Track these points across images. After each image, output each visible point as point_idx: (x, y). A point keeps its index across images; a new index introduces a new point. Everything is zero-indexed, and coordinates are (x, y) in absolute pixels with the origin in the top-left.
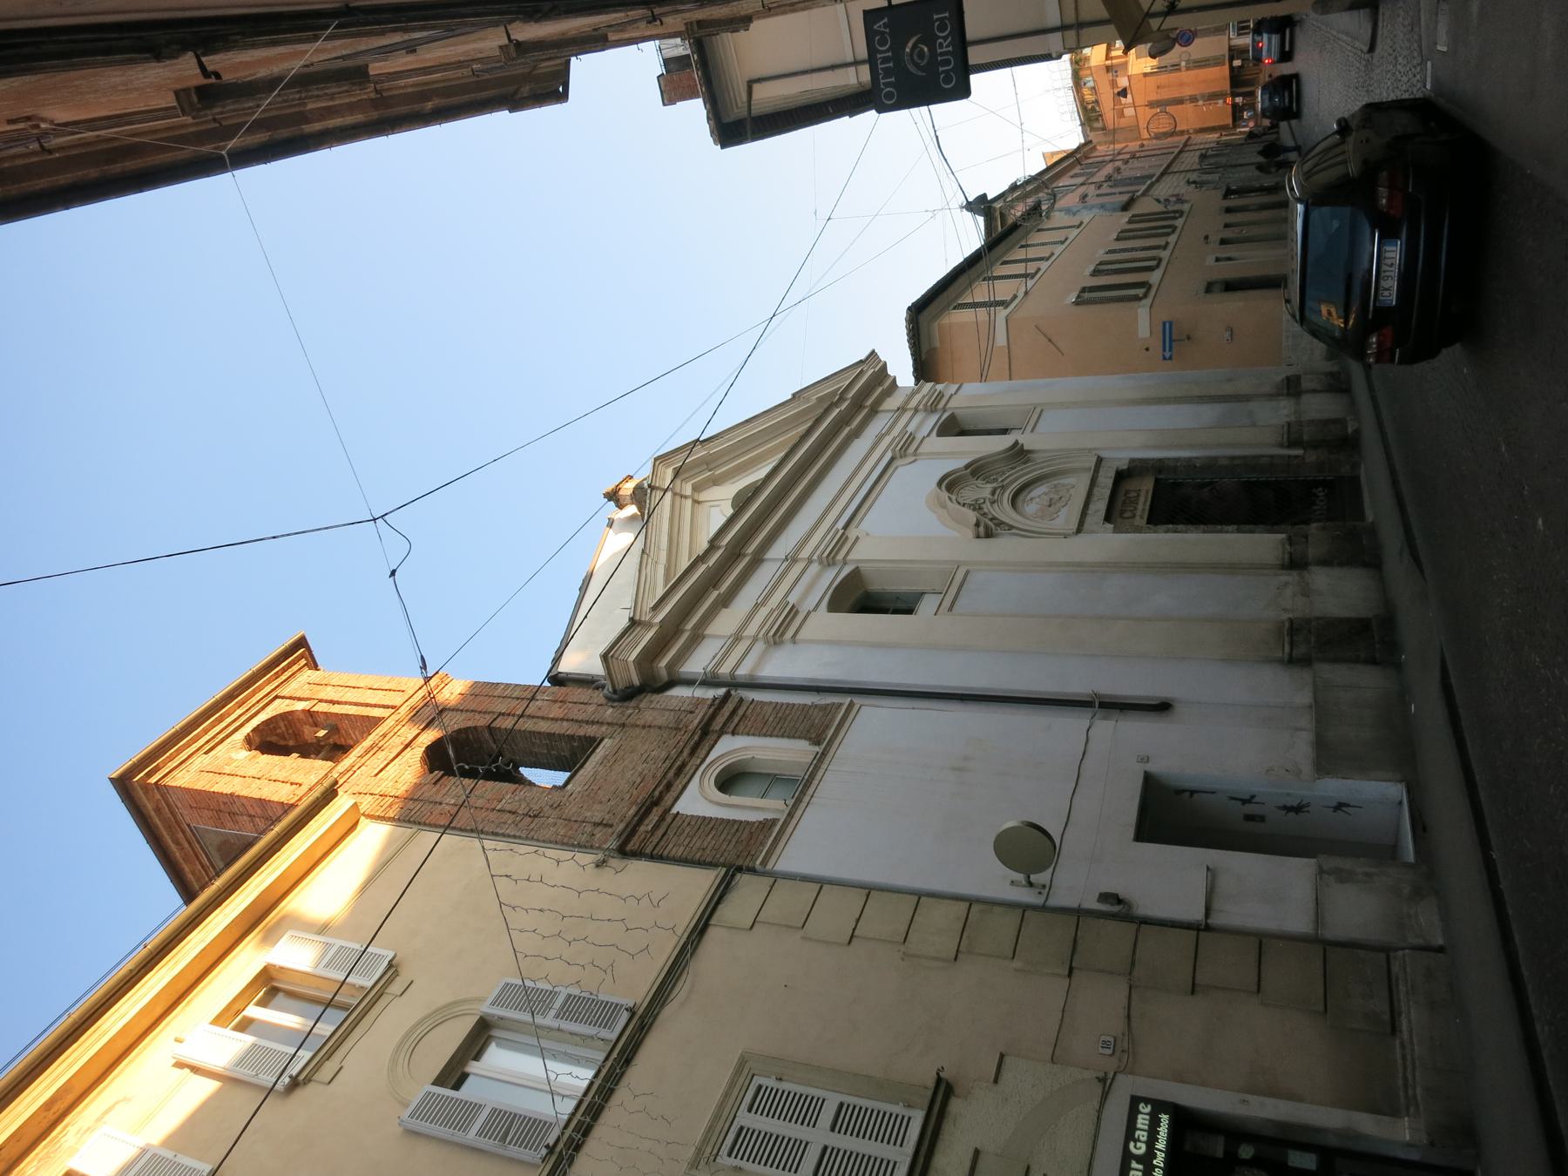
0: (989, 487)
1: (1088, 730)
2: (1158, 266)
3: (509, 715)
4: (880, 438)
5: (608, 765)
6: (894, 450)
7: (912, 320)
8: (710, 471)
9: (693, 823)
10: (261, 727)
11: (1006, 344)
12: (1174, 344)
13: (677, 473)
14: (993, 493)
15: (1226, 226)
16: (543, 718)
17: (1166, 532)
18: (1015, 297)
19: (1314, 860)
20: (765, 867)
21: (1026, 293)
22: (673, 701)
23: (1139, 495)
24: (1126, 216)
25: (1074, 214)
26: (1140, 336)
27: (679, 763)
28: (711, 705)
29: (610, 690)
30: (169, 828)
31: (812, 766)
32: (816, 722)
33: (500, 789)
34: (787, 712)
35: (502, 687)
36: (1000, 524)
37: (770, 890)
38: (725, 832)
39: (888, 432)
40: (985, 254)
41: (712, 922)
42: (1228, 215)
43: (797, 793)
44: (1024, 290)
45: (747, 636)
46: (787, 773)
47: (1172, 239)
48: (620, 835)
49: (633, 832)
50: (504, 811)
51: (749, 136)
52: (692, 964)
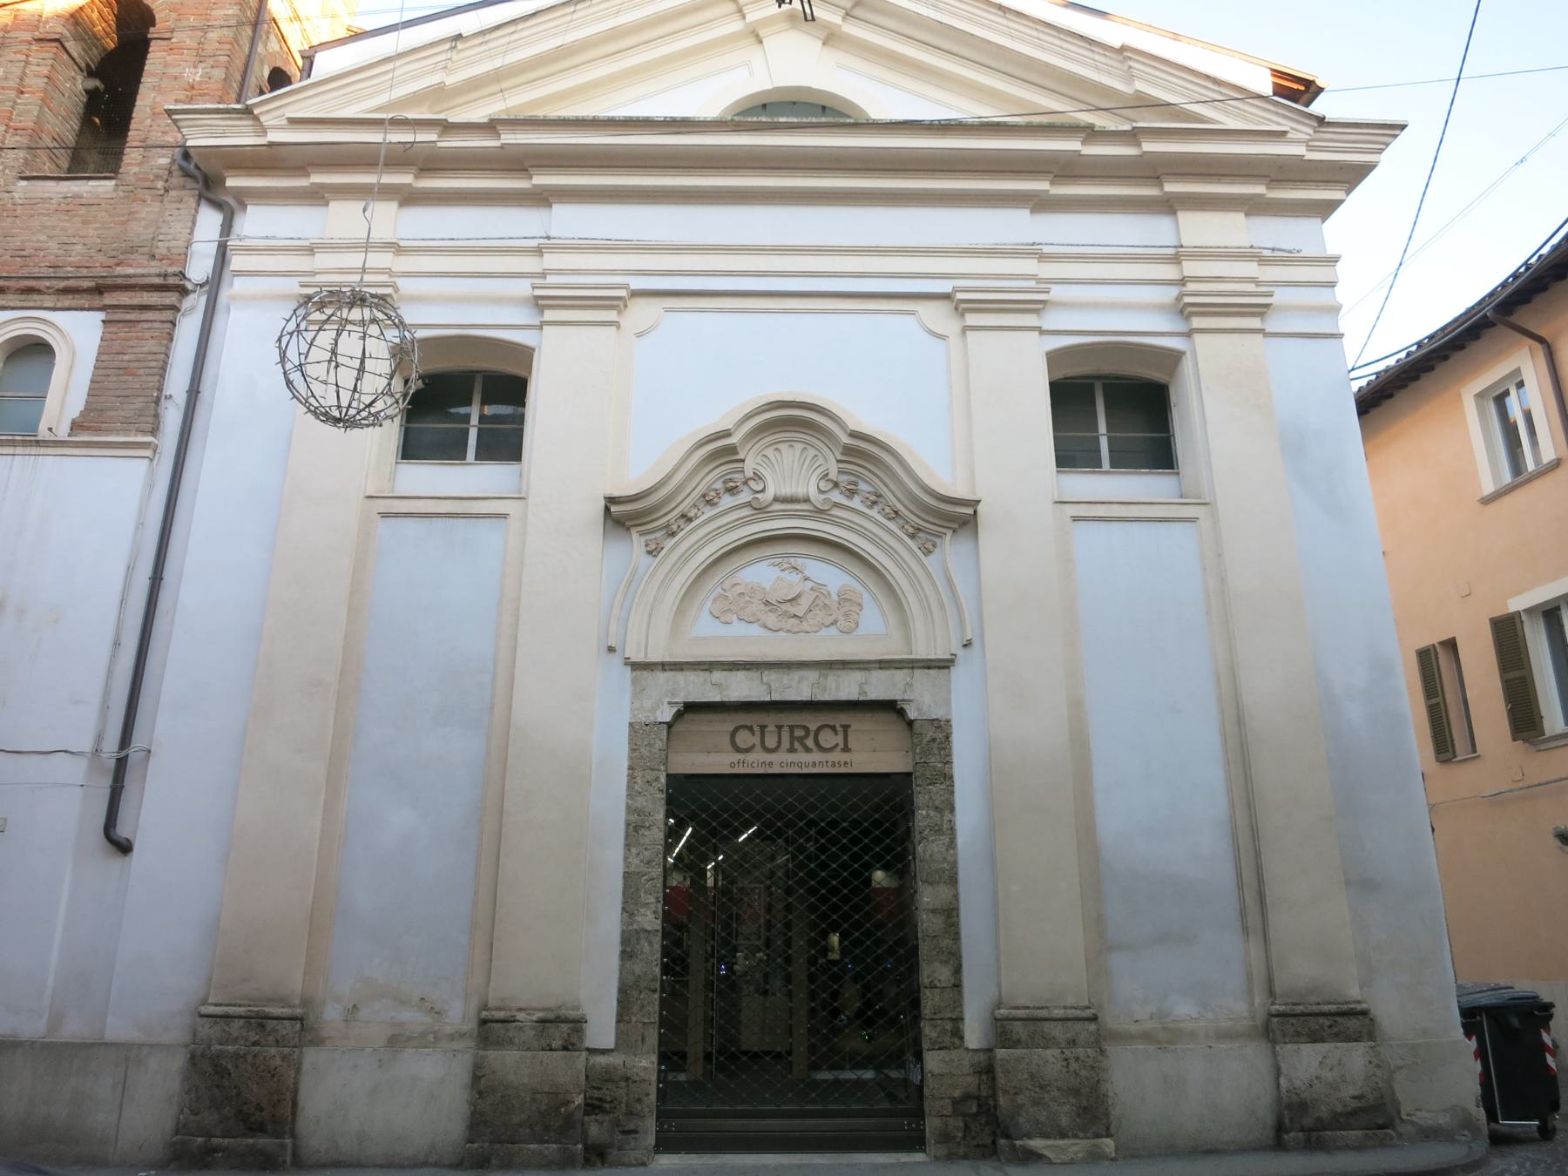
1: (65, 751)
31: (10, 438)
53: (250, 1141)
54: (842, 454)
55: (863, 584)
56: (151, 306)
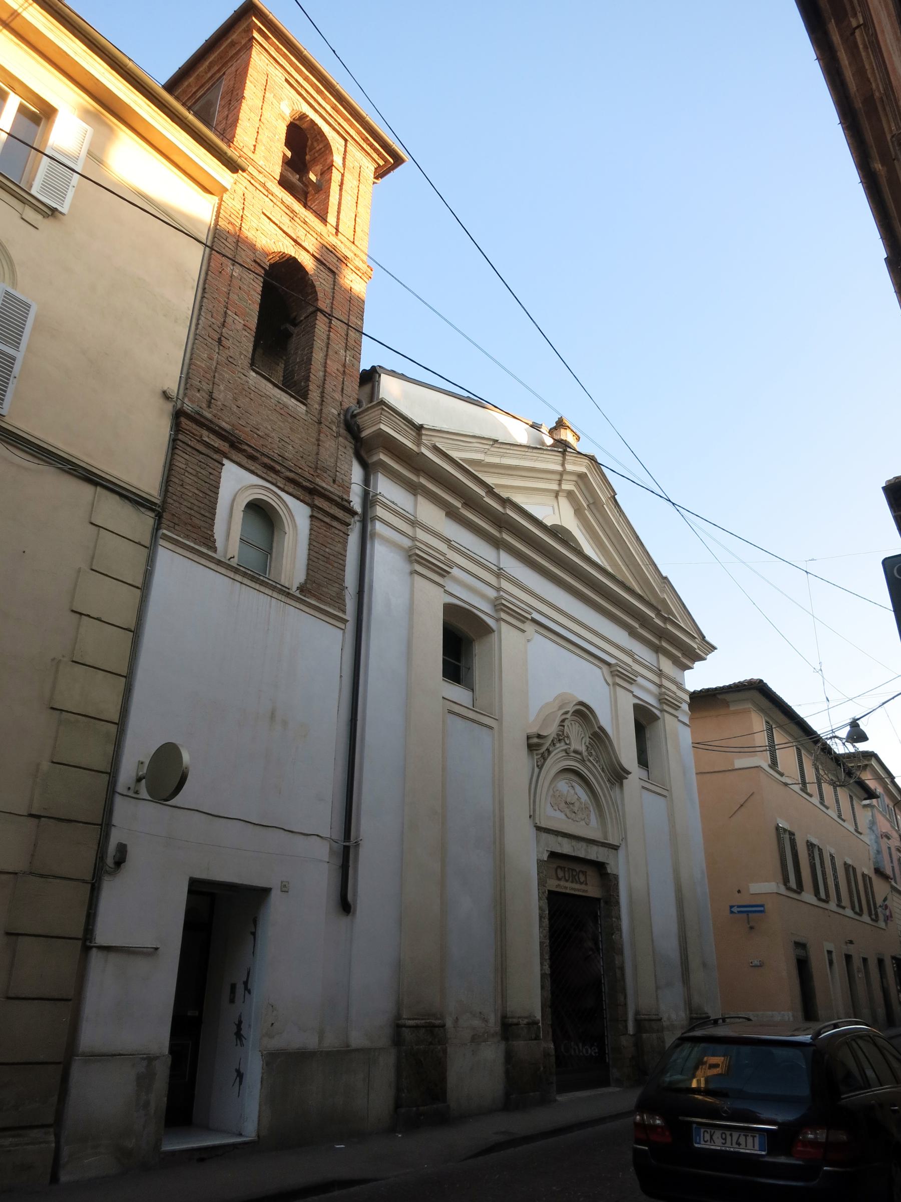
0: (583, 749)
1: (318, 836)
2: (820, 899)
3: (330, 327)
4: (629, 654)
5: (278, 409)
6: (617, 665)
7: (752, 684)
8: (588, 506)
9: (211, 477)
10: (315, 127)
11: (736, 767)
12: (745, 915)
13: (582, 476)
14: (576, 752)
15: (865, 960)
16: (327, 355)
17: (540, 908)
18: (782, 775)
19: (167, 1053)
20: (161, 538)
21: (786, 784)
22: (347, 466)
23: (581, 883)
24: (869, 871)
25: (871, 828)
26: (750, 885)
27: (278, 467)
28: (342, 499)
29: (355, 412)
30: (220, 57)
31: (274, 584)
32: (324, 589)
33: (251, 315)
34: (336, 565)
35: (359, 323)
36: (544, 758)
37: (136, 543)
38: (200, 504)
39: (635, 660)
40: (811, 739)
41: (99, 488)
42: (876, 961)
43: (244, 570)
44: (789, 781)
45: (500, 582)
46: (273, 564)
47: (849, 912)
48: (199, 414)
49: (201, 425)
50: (225, 317)
51: (896, 514)
52: (52, 469)
53: (435, 1106)
54: (591, 734)
55: (591, 801)
56: (339, 518)
